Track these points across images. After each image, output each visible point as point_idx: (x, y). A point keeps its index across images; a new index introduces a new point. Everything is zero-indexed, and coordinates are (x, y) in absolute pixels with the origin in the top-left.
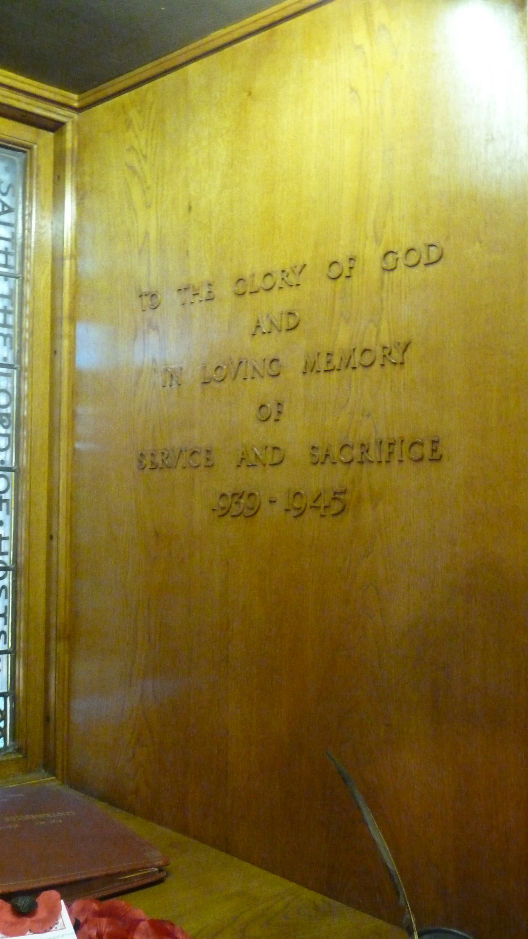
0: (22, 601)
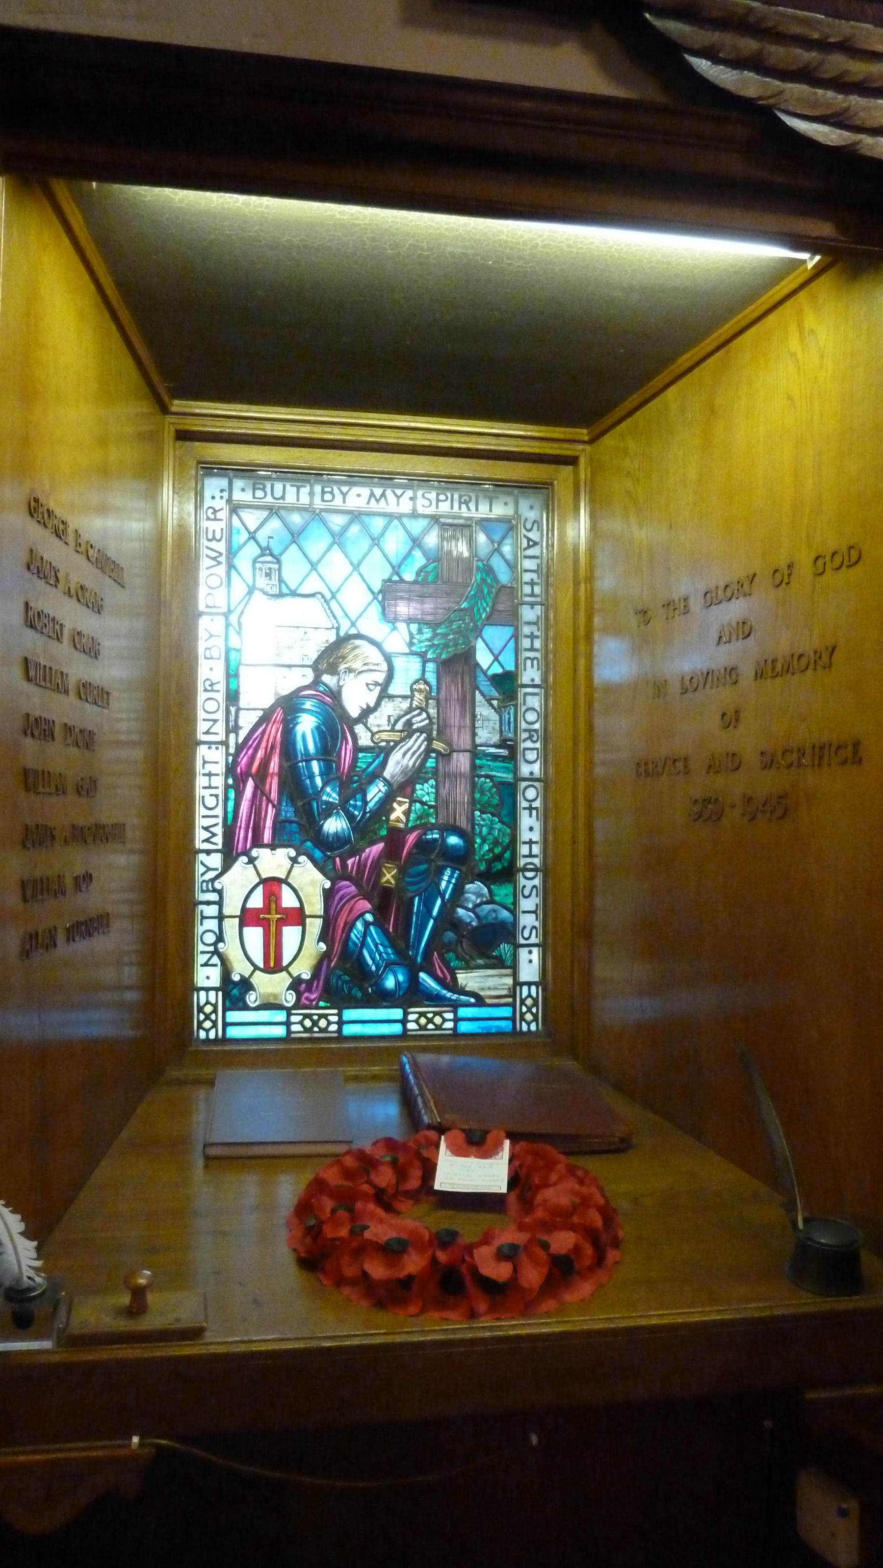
0: (550, 900)
